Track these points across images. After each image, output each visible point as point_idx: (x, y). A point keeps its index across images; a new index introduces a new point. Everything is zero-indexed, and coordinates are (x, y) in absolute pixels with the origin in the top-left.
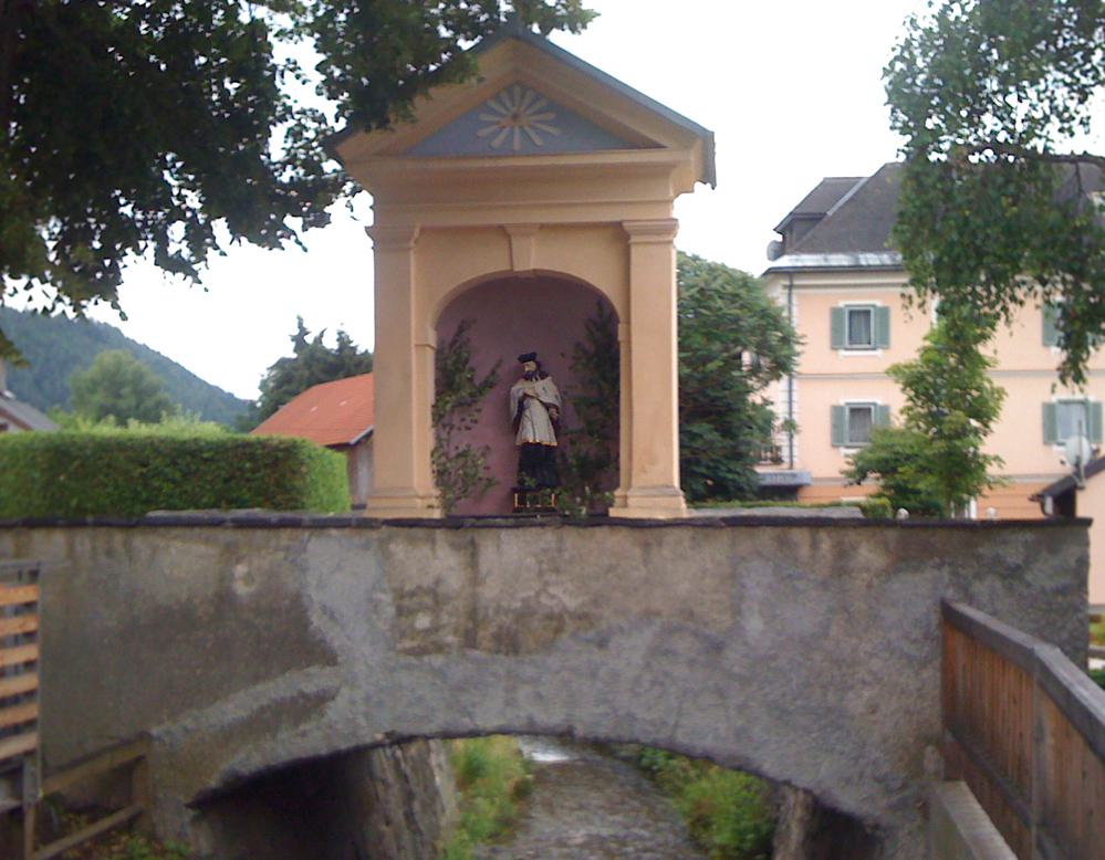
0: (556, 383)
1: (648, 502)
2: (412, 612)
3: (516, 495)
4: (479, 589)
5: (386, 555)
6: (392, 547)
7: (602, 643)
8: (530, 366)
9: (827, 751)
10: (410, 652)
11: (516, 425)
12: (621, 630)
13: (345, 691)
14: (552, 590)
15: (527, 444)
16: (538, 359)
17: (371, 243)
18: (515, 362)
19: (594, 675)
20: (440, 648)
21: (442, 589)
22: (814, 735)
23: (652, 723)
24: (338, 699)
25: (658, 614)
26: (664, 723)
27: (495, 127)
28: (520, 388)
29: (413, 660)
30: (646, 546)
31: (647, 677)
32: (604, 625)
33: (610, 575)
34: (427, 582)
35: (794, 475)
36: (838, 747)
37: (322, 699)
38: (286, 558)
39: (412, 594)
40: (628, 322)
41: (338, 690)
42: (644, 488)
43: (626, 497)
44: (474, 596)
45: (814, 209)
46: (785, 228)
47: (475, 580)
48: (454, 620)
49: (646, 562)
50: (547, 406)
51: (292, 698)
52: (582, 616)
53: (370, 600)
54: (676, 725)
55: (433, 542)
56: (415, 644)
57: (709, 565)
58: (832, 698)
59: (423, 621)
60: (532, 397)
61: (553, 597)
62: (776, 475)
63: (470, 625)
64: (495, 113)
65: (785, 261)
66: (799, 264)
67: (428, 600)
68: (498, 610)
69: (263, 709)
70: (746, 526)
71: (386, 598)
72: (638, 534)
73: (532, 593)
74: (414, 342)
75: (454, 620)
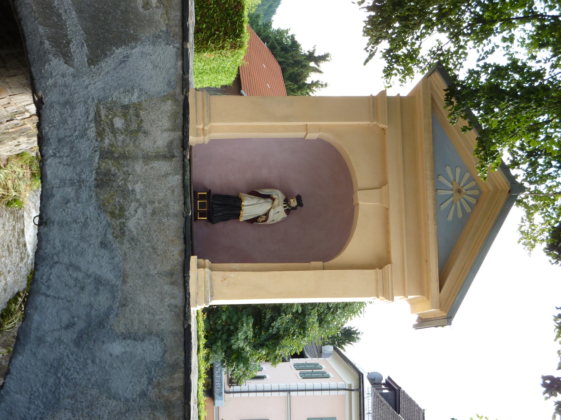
0: (283, 220)
1: (201, 283)
2: (125, 115)
3: (206, 193)
4: (141, 162)
5: (164, 99)
6: (169, 102)
7: (104, 245)
8: (293, 203)
9: (30, 398)
10: (98, 114)
11: (254, 193)
12: (113, 258)
13: (71, 70)
14: (140, 211)
15: (241, 201)
16: (298, 207)
17: (375, 94)
18: (297, 192)
19: (82, 238)
20: (100, 134)
21: (141, 135)
22: (40, 389)
23: (49, 279)
24: (66, 66)
25: (124, 282)
26: (48, 287)
27: (452, 178)
28: (279, 196)
29: (91, 117)
30: (171, 274)
31: (80, 276)
32: (116, 245)
33: (151, 249)
34: (146, 126)
35: (221, 394)
36: (33, 406)
37: (67, 57)
38: (161, 31)
39: (137, 116)
40: (324, 268)
41: (72, 66)
42: (211, 279)
43: (204, 267)
44: (135, 158)
45: (402, 405)
46: (390, 384)
47: (147, 158)
48: (120, 144)
49: (160, 274)
50: (267, 215)
51: (66, 35)
52: (122, 231)
53: (133, 88)
54: (47, 296)
55: (173, 130)
56: (103, 118)
57: (157, 317)
58: (67, 402)
59: (119, 123)
60: (273, 203)
61: (136, 211)
62: (221, 382)
63: (116, 155)
64: (462, 177)
65: (367, 386)
66: (365, 395)
67: (134, 126)
68: (127, 174)
69: (59, 16)
70: (185, 342)
71: (135, 98)
72: (179, 269)
73: (138, 197)
74: (309, 123)
75: (120, 144)
